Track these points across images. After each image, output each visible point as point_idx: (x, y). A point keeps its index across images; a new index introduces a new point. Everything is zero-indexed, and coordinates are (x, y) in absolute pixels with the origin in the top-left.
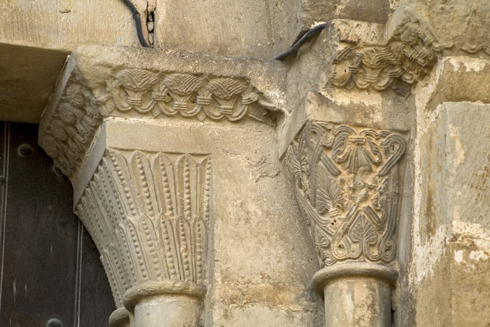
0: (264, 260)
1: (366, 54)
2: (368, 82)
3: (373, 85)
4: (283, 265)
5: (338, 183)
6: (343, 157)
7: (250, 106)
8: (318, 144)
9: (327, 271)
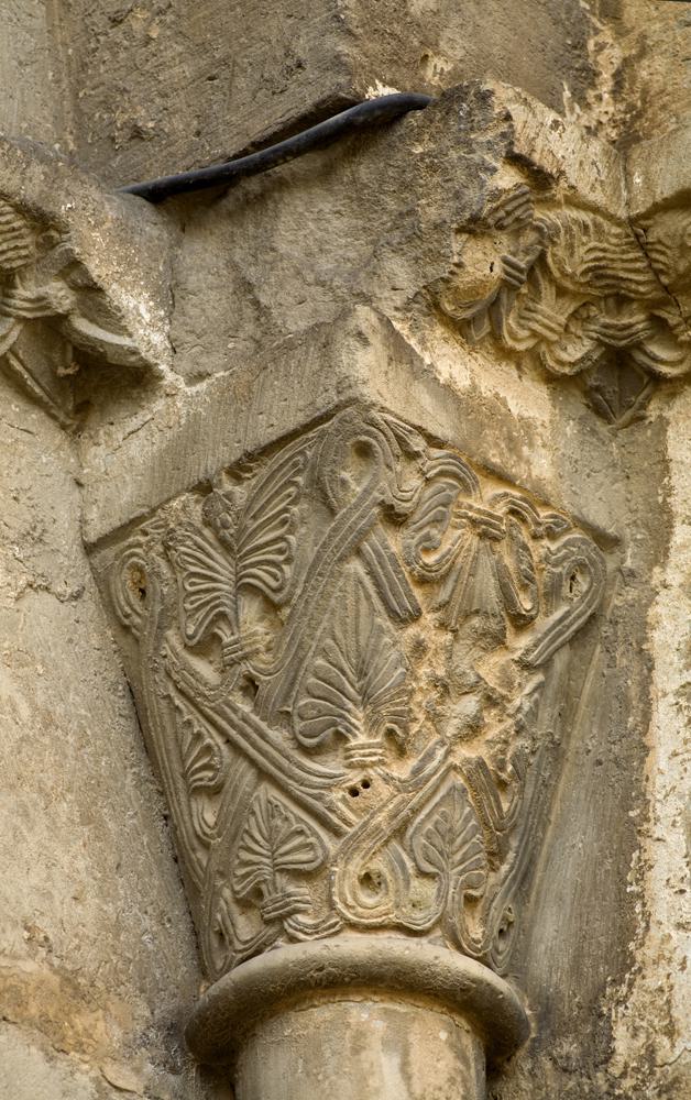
0: (34, 880)
1: (568, 230)
2: (534, 334)
3: (543, 348)
4: (87, 913)
5: (406, 650)
6: (438, 562)
7: (19, 328)
8: (367, 492)
9: (325, 952)
